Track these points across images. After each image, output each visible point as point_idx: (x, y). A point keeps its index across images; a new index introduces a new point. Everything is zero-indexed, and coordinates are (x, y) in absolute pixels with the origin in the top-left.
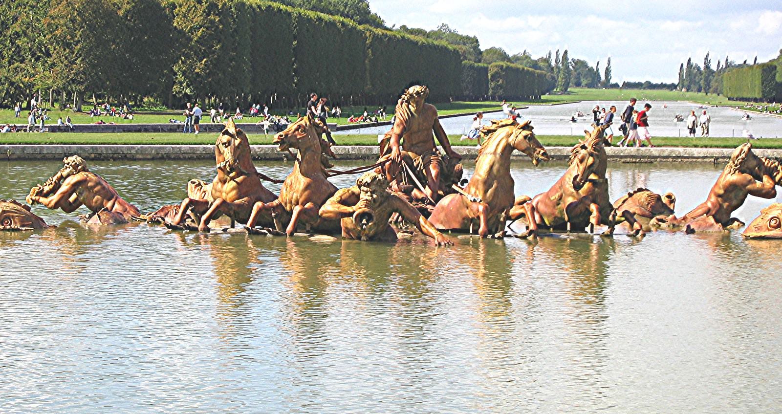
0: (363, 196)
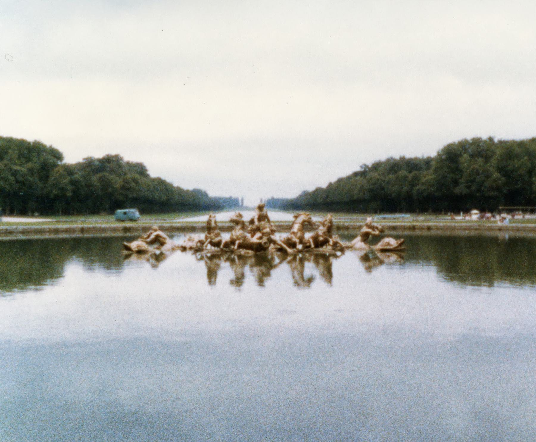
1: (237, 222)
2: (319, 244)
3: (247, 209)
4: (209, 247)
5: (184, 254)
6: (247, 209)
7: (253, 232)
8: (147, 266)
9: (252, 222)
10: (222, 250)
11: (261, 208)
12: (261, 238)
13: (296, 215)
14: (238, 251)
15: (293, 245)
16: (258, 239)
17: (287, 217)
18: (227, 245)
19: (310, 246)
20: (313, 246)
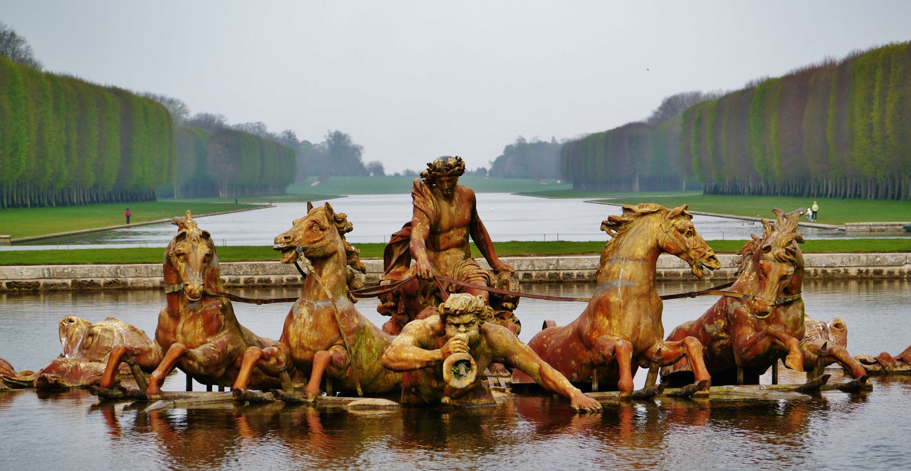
0: (450, 331)
1: (317, 251)
2: (732, 363)
3: (375, 181)
4: (177, 382)
5: (25, 370)
6: (375, 181)
7: (403, 304)
8: (816, 423)
9: (397, 250)
10: (240, 399)
11: (443, 179)
12: (438, 337)
13: (617, 211)
14: (285, 413)
15: (603, 373)
16: (423, 345)
17: (579, 219)
18: (266, 376)
19: (690, 377)
20: (703, 374)
